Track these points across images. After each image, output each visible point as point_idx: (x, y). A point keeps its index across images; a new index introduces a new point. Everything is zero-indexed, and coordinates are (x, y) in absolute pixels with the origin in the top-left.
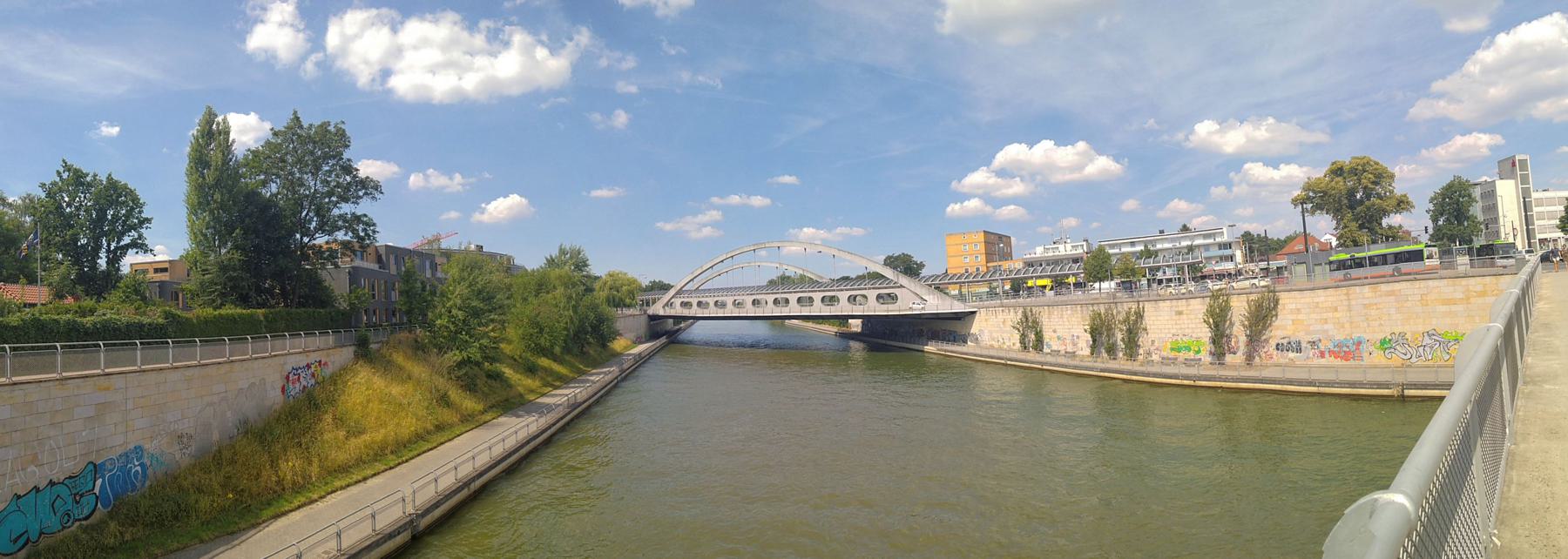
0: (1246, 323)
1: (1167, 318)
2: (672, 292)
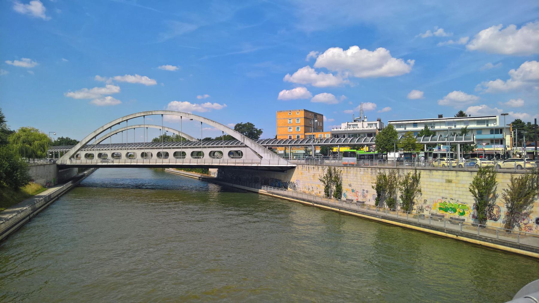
0: (509, 197)
1: (438, 184)
2: (78, 146)
